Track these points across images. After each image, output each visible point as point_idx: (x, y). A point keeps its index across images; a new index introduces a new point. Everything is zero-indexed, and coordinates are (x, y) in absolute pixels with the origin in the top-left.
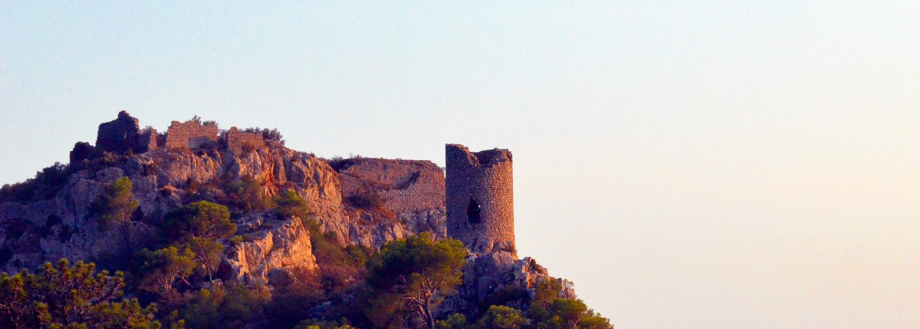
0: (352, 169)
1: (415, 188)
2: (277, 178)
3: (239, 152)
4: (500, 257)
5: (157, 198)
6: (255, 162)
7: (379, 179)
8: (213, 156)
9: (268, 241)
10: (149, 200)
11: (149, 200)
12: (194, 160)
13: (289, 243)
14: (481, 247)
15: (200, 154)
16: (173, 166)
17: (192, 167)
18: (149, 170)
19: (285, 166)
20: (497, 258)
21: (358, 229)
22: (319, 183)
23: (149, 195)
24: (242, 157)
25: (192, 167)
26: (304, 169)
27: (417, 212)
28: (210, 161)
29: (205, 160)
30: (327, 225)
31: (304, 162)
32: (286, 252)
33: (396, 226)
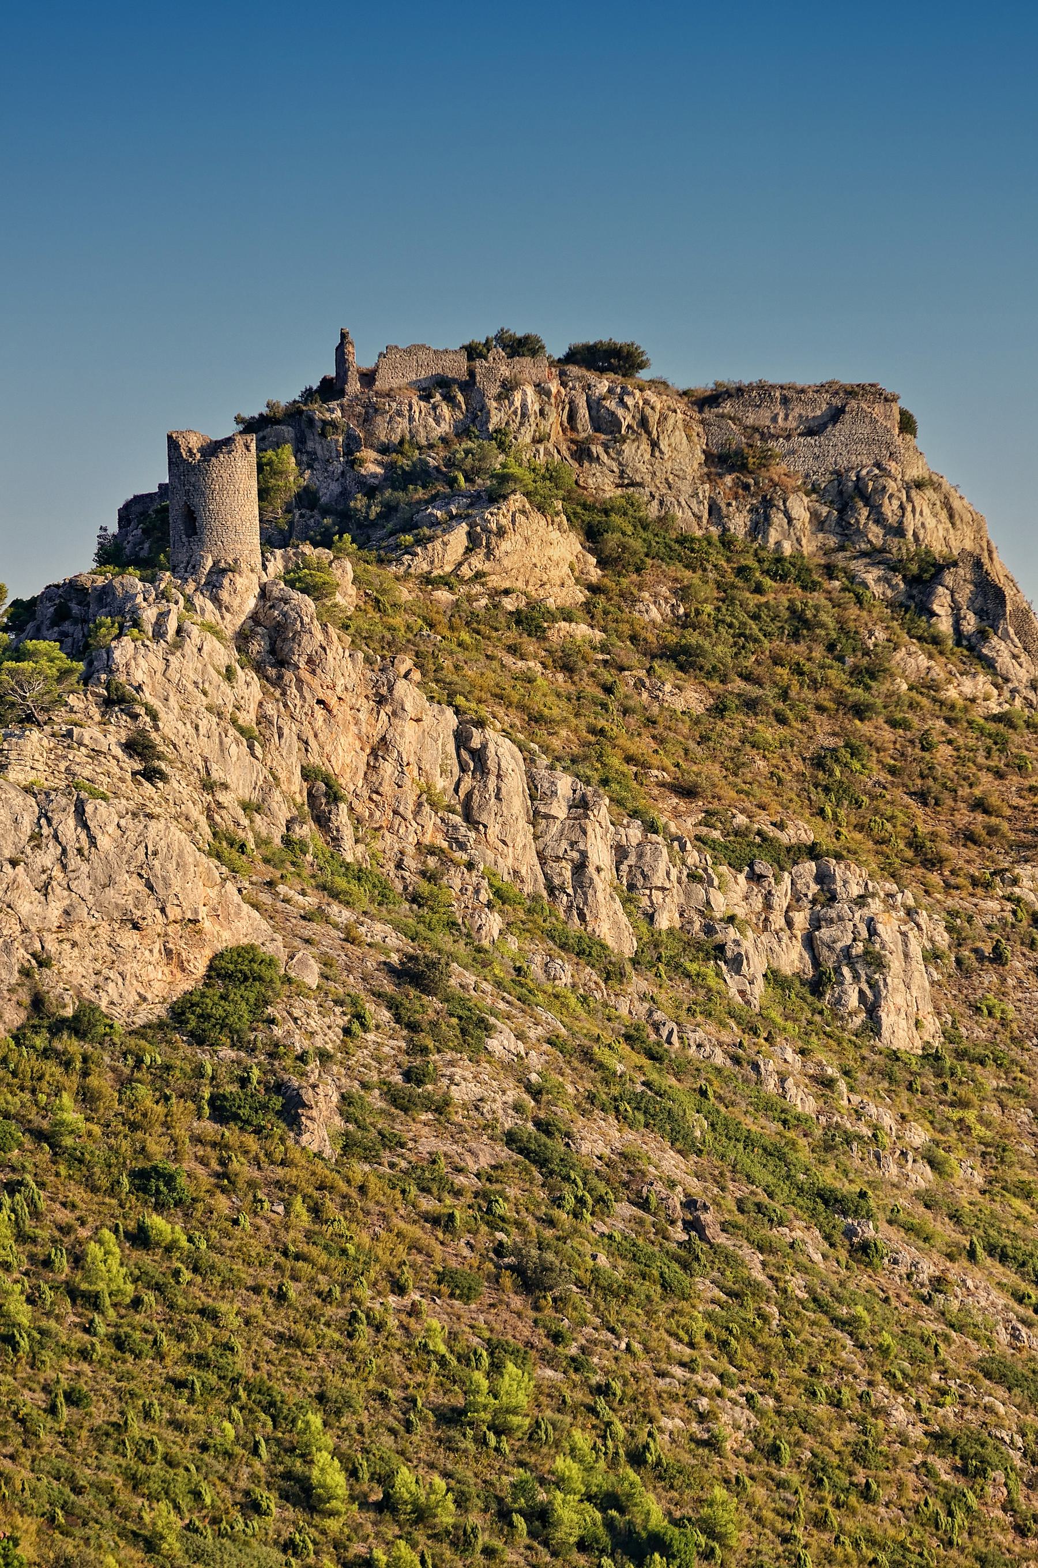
0: (727, 408)
1: (839, 432)
2: (574, 429)
3: (494, 390)
4: (122, 584)
5: (343, 472)
6: (524, 405)
7: (774, 419)
8: (449, 399)
9: (458, 537)
10: (331, 476)
11: (331, 476)
12: (416, 408)
13: (494, 539)
14: (194, 567)
15: (426, 397)
16: (379, 419)
17: (411, 419)
18: (329, 428)
19: (590, 408)
20: (117, 585)
21: (723, 506)
22: (649, 433)
23: (330, 468)
24: (499, 398)
25: (411, 419)
26: (620, 412)
27: (837, 473)
28: (445, 410)
29: (434, 408)
30: (661, 503)
31: (621, 400)
32: (489, 554)
33: (792, 497)
